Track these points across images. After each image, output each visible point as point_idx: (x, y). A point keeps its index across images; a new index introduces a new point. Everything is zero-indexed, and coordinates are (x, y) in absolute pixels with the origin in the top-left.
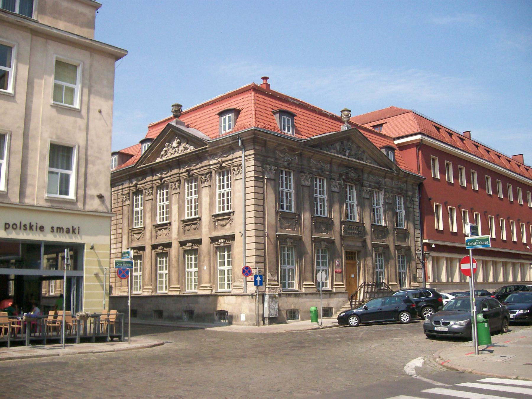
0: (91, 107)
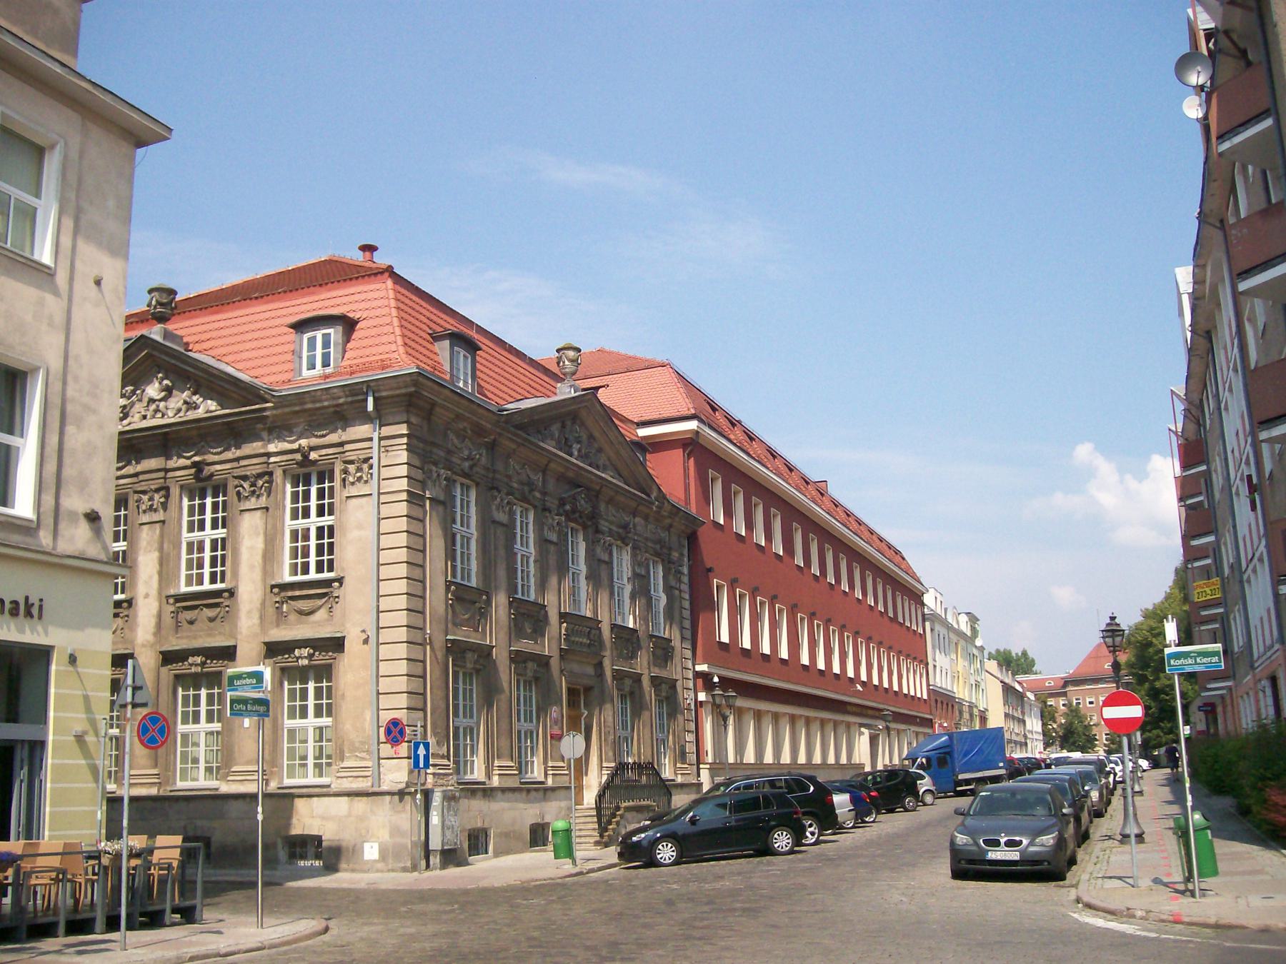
0: (79, 265)
